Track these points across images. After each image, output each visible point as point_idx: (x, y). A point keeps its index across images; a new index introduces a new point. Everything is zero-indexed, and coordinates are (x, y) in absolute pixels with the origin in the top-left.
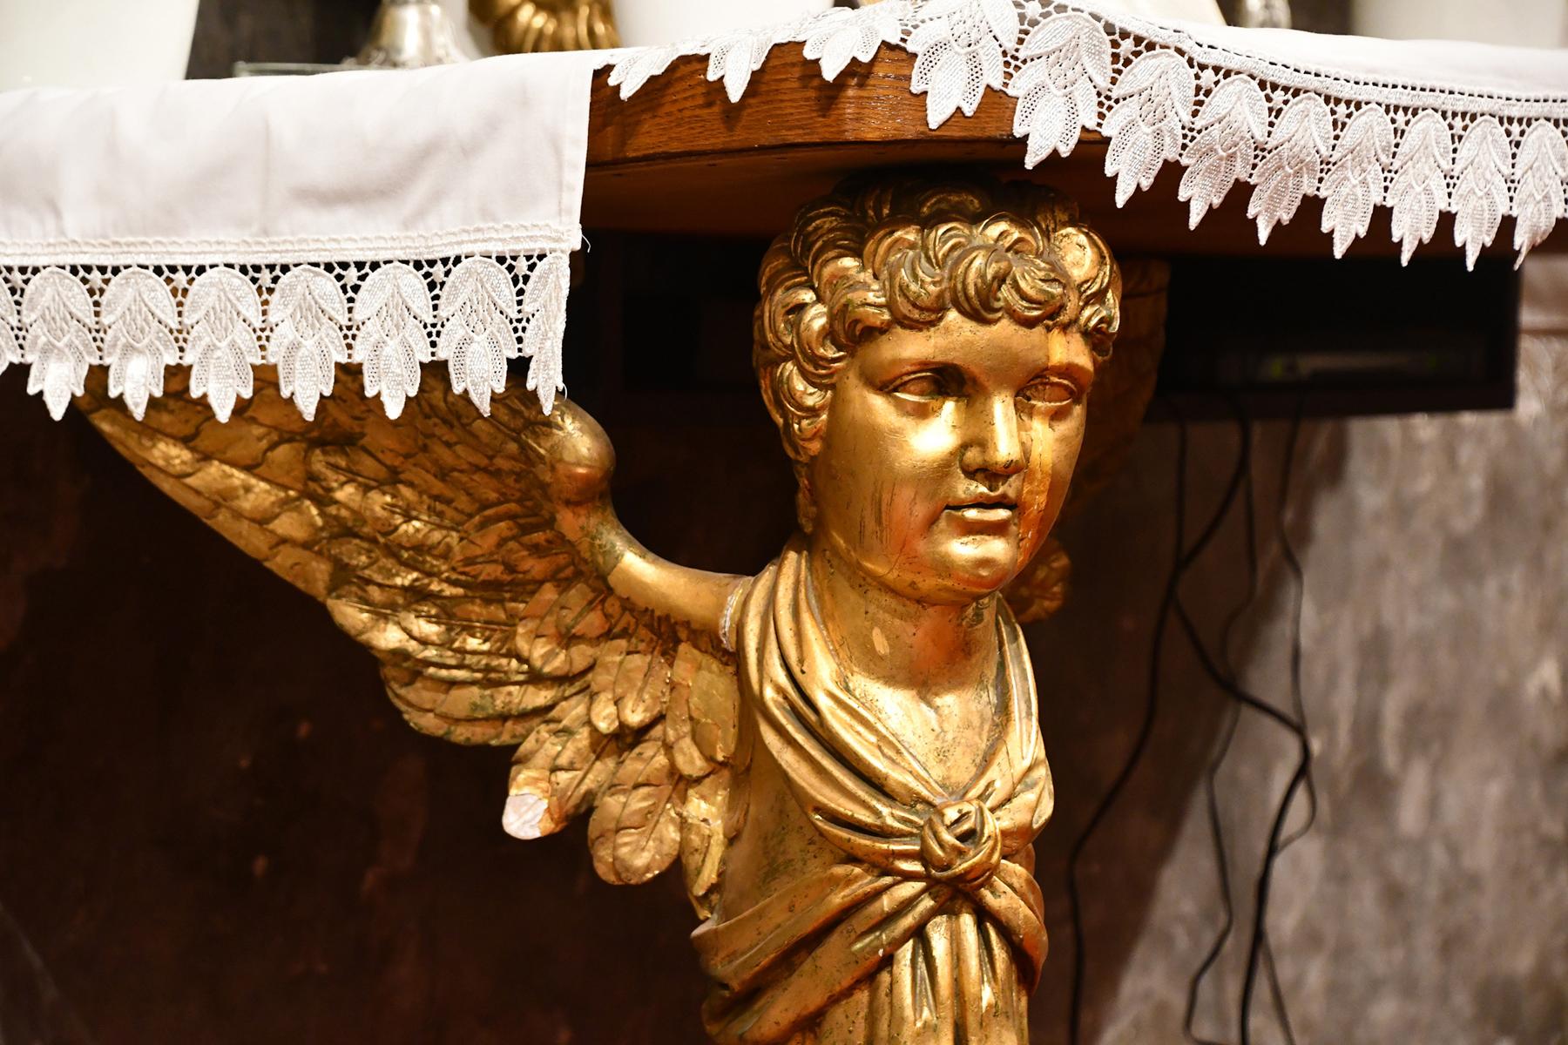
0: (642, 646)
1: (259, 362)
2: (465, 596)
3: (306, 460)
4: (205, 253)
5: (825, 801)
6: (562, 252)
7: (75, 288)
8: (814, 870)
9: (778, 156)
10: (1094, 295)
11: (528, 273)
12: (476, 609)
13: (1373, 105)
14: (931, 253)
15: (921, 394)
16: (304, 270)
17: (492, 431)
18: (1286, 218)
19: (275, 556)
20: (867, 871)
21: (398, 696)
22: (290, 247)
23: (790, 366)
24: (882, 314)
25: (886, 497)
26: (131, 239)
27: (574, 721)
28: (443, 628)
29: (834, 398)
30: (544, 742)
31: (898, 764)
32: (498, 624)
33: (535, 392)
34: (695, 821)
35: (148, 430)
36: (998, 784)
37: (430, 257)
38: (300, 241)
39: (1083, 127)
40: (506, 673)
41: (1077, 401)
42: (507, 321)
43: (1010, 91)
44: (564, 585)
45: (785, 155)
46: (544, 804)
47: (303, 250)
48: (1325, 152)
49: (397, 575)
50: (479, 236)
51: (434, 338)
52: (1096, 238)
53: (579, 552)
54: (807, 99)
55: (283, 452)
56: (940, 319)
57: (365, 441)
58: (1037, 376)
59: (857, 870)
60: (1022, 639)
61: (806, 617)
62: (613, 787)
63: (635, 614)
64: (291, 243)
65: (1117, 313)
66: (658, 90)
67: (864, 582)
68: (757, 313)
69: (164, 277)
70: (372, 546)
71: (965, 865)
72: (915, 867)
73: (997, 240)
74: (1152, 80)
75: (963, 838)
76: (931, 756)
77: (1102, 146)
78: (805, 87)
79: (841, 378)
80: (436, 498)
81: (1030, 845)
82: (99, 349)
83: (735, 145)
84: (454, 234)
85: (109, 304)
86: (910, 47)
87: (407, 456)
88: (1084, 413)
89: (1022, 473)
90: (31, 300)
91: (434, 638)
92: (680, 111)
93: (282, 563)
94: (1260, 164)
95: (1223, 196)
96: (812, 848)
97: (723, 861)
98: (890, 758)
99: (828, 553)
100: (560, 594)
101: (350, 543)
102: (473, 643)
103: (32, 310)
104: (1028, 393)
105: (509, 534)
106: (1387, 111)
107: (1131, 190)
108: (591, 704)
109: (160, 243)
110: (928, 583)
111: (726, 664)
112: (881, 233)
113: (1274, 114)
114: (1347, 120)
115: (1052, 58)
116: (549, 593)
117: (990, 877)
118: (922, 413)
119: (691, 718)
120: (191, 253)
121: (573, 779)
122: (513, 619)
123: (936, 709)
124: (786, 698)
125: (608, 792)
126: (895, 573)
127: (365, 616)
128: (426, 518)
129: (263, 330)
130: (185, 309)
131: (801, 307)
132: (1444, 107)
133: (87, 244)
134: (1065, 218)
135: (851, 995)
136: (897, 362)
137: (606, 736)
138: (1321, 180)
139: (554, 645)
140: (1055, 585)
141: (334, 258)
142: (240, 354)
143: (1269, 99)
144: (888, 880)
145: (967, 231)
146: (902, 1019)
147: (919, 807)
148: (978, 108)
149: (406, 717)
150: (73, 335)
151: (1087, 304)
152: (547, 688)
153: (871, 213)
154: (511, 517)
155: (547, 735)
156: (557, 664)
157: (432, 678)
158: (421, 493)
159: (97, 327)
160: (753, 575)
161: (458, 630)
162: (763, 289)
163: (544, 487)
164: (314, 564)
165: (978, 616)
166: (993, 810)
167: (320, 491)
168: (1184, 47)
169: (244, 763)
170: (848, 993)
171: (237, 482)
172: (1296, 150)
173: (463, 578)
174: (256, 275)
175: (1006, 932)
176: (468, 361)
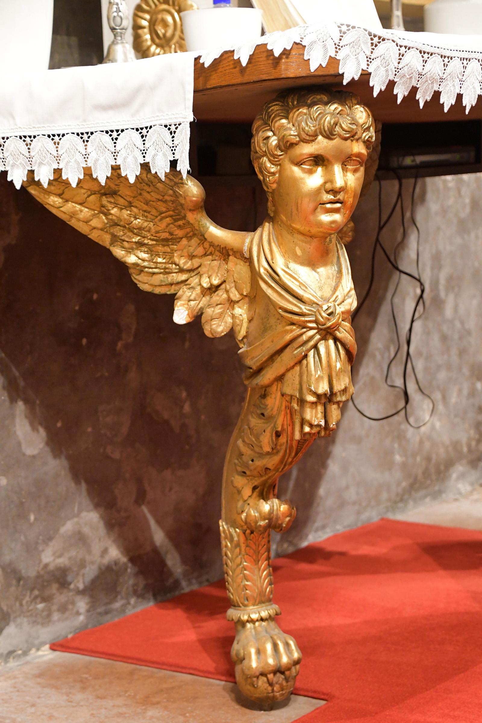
0: (217, 258)
1: (85, 166)
2: (156, 244)
3: (100, 200)
4: (64, 129)
5: (283, 305)
6: (187, 122)
7: (21, 143)
8: (280, 328)
9: (260, 84)
10: (367, 128)
11: (176, 130)
12: (160, 248)
13: (456, 58)
14: (312, 116)
15: (310, 165)
16: (98, 133)
17: (164, 186)
18: (429, 99)
19: (92, 233)
20: (297, 327)
21: (135, 279)
22: (93, 126)
23: (265, 158)
24: (296, 138)
25: (300, 202)
26: (39, 126)
27: (195, 284)
28: (149, 255)
29: (281, 168)
30: (185, 292)
31: (306, 292)
32: (168, 253)
33: (180, 171)
34: (238, 315)
35: (47, 192)
36: (339, 297)
37: (141, 127)
38: (97, 123)
39: (362, 69)
40: (171, 269)
41: (362, 166)
42: (169, 147)
43: (338, 58)
44: (189, 238)
45: (261, 84)
46: (187, 312)
47: (98, 127)
48: (441, 75)
49: (133, 238)
50: (158, 118)
51: (144, 154)
52: (366, 108)
53: (194, 227)
54: (269, 64)
55: (92, 197)
56: (316, 139)
57: (119, 193)
58: (348, 158)
59: (294, 327)
60: (344, 248)
61: (273, 245)
62: (209, 306)
63: (214, 247)
64: (94, 124)
65: (374, 134)
66: (217, 63)
67: (292, 231)
68: (252, 141)
69: (51, 138)
70: (124, 229)
71: (330, 324)
72: (314, 325)
73: (334, 111)
74: (384, 51)
75: (329, 315)
76: (317, 289)
77: (368, 76)
78: (268, 59)
79: (283, 162)
80: (145, 211)
81: (350, 317)
82: (31, 164)
83: (245, 81)
84: (149, 118)
85: (33, 149)
86: (303, 44)
87: (134, 197)
88: (364, 169)
89: (344, 191)
90: (7, 149)
91: (147, 259)
92: (225, 70)
93: (94, 236)
94: (420, 80)
95: (408, 92)
96: (278, 321)
97: (248, 328)
98: (304, 291)
99: (279, 222)
100: (188, 241)
101: (116, 228)
102: (160, 260)
103: (7, 152)
104: (345, 164)
105: (170, 222)
106: (461, 60)
107: (378, 91)
108: (200, 278)
109: (49, 126)
110: (314, 231)
111: (246, 262)
112: (295, 110)
113: (424, 62)
114: (448, 63)
115: (351, 45)
116: (184, 242)
117: (338, 327)
118: (311, 172)
119: (234, 281)
120: (60, 130)
121: (196, 303)
122: (172, 251)
123: (318, 273)
124: (268, 272)
125: (208, 307)
126: (303, 227)
127: (123, 252)
128: (142, 218)
129: (86, 155)
130: (59, 149)
131: (268, 138)
132: (479, 58)
133: (24, 128)
134: (356, 102)
135: (293, 368)
136: (302, 155)
137: (206, 289)
138: (440, 85)
139: (187, 259)
140: (349, 232)
141: (108, 129)
142: (78, 164)
143: (423, 57)
144: (305, 330)
145: (324, 108)
146: (311, 375)
147: (314, 305)
148: (327, 64)
149: (138, 286)
150: (22, 160)
151: (364, 132)
152: (185, 274)
153: (290, 103)
154: (171, 216)
155: (186, 290)
156: (188, 266)
157: (147, 272)
158: (139, 210)
159: (29, 157)
160: (254, 232)
161: (154, 256)
162: (254, 133)
163: (182, 205)
164: (105, 236)
165: (331, 241)
166: (338, 305)
167: (106, 211)
168: (395, 40)
169: (77, 308)
170: (293, 367)
171: (78, 209)
172: (432, 74)
173: (155, 238)
174: (82, 136)
175: (344, 345)
176: (156, 162)
